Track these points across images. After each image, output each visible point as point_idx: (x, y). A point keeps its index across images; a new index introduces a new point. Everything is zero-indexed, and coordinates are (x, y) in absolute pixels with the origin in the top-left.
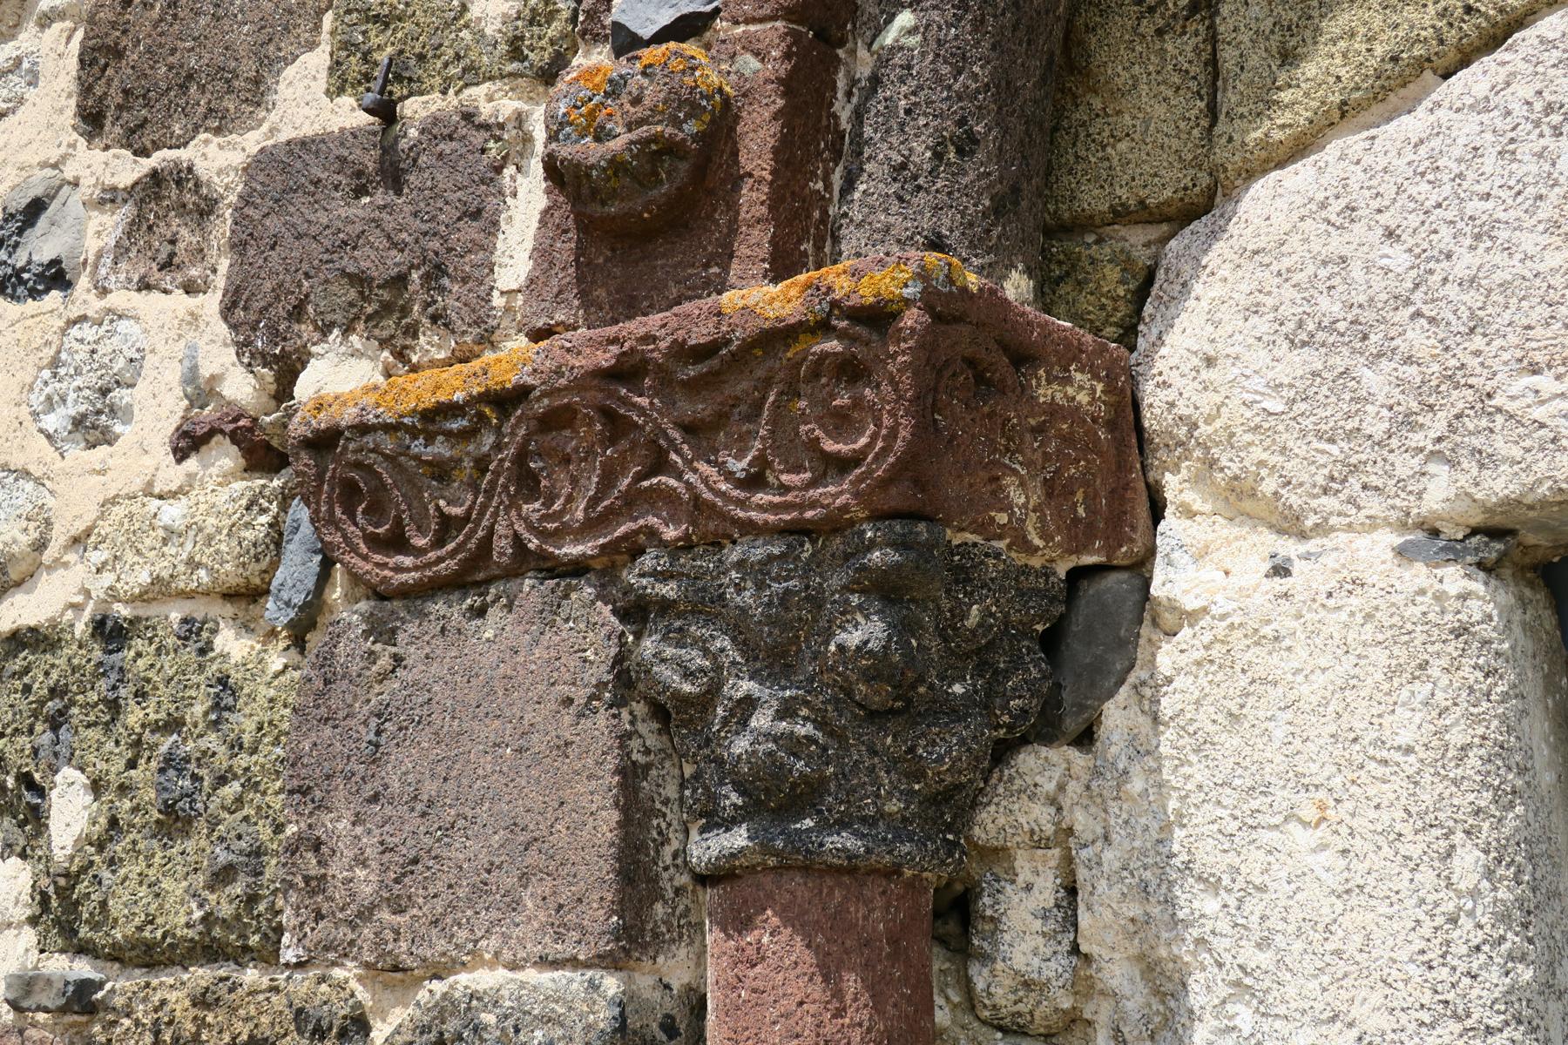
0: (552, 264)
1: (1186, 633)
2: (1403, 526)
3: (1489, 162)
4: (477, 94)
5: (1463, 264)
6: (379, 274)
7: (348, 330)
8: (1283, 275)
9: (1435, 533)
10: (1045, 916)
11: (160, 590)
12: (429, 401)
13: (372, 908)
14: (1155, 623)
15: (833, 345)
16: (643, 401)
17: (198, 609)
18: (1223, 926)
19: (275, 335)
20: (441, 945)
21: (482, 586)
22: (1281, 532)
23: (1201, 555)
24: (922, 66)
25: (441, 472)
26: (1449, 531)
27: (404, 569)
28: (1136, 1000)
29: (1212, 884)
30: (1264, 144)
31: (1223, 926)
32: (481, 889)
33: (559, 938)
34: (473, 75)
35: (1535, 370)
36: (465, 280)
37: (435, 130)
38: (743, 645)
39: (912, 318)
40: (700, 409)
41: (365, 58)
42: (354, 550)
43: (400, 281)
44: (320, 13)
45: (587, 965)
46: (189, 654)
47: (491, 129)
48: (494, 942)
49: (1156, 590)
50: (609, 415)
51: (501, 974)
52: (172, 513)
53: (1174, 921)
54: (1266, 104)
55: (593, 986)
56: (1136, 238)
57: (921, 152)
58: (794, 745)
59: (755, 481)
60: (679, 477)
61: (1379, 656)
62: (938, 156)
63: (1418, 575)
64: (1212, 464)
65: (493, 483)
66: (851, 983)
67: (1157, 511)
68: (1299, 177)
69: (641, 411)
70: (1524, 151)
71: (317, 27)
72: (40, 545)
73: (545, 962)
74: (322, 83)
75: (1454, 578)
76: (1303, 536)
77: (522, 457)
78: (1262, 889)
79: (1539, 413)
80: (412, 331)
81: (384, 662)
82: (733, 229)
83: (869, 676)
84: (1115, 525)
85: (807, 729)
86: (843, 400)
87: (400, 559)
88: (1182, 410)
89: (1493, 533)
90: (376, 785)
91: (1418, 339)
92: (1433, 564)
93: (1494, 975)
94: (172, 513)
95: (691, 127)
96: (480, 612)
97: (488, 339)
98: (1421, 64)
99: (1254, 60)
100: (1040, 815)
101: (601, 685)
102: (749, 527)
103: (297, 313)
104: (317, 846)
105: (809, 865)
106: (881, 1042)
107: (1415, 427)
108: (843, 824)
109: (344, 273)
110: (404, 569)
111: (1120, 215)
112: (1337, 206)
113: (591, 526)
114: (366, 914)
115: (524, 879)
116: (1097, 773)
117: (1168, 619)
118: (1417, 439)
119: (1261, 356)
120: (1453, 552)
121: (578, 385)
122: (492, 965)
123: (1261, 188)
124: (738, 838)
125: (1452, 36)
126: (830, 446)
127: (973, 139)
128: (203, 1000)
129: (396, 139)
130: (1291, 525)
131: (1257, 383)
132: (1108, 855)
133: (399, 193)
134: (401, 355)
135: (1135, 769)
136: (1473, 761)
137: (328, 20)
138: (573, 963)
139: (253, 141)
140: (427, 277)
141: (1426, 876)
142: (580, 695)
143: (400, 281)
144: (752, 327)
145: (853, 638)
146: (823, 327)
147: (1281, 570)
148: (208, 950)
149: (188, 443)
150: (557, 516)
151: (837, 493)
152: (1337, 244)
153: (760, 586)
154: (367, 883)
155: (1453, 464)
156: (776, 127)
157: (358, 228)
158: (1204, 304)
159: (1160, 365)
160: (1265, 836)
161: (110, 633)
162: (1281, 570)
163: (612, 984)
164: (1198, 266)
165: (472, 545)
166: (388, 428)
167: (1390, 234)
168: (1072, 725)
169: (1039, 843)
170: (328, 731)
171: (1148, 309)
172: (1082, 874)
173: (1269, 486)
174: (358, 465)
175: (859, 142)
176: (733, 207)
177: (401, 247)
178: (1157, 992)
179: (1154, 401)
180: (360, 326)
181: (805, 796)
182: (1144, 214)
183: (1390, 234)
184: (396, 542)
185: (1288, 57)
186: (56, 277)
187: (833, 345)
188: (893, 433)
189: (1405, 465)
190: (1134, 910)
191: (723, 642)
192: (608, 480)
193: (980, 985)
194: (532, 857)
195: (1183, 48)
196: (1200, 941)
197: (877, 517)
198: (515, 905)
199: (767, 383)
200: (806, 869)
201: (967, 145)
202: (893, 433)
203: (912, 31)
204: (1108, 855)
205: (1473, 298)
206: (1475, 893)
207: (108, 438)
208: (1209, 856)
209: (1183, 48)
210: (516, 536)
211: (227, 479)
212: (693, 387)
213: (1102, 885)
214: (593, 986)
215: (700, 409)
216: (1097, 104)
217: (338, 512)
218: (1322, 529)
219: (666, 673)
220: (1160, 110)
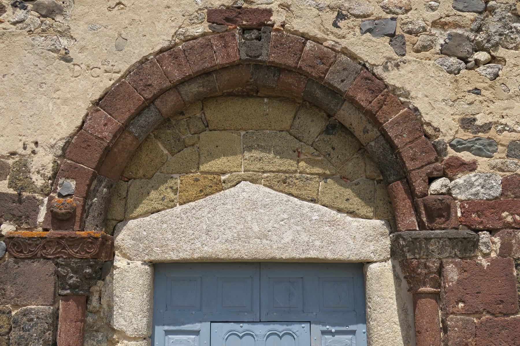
0: (47, 220)
1: (117, 269)
2: (142, 261)
3: (155, 225)
5: (152, 235)
6: (17, 215)
7: (10, 221)
8: (133, 232)
9: (145, 262)
10: (97, 299)
12: (31, 236)
13: (13, 298)
14: (113, 268)
15: (90, 240)
16: (63, 242)
18: (119, 301)
20: (25, 303)
21: (34, 259)
22: (129, 259)
23: (119, 261)
24: (97, 205)
26: (147, 262)
27: (22, 255)
29: (118, 297)
30: (132, 217)
31: (119, 301)
33: (44, 302)
35: (157, 247)
36: (32, 219)
37: (28, 198)
38: (71, 270)
39: (100, 239)
40: (71, 243)
41: (16, 184)
42: (14, 252)
43: (21, 217)
44: (7, 175)
45: (48, 305)
48: (34, 302)
49: (114, 264)
50: (58, 242)
51: (35, 306)
53: (113, 301)
54: (132, 212)
55: (50, 308)
56: (114, 223)
57: (96, 215)
58: (78, 282)
59: (77, 253)
60: (67, 251)
61: (139, 274)
62: (98, 215)
63: (143, 267)
64: (122, 251)
65: (39, 248)
66: (80, 308)
67: (114, 255)
68: (135, 221)
69: (63, 243)
70: (159, 225)
71: (6, 177)
73: (42, 305)
74: (7, 186)
75: (147, 267)
76: (131, 260)
77: (44, 245)
78: (123, 298)
79: (157, 252)
80: (22, 223)
81: (17, 266)
82: (75, 222)
83: (88, 275)
84: (110, 257)
85: (79, 280)
86: (90, 246)
87: (21, 254)
88: (119, 244)
89: (151, 262)
90: (15, 282)
91: (146, 242)
92: (145, 265)
93: (146, 307)
95: (72, 210)
96: (34, 262)
97: (36, 227)
98: (149, 212)
99: (131, 207)
100: (98, 288)
101: (52, 273)
102: (76, 258)
104: (4, 289)
105: (77, 295)
107: (145, 251)
108: (81, 290)
109: (10, 213)
111: (113, 219)
112: (139, 226)
113: (53, 254)
114: (12, 298)
115: (39, 295)
116: (105, 284)
117: (115, 268)
118: (145, 252)
119: (129, 241)
120: (147, 264)
121: (55, 238)
122: (33, 305)
123: (131, 222)
124: (69, 291)
125: (153, 210)
126: (88, 251)
127: (102, 213)
129: (21, 197)
130: (130, 259)
131: (128, 243)
132: (106, 293)
133: (21, 205)
134: (19, 226)
135: (110, 284)
136: (147, 286)
137: (8, 177)
138: (47, 305)
140: (25, 217)
141: (141, 297)
142: (49, 274)
143: (21, 217)
144: (80, 237)
146: (89, 238)
147: (129, 264)
150: (48, 252)
151: (88, 256)
152: (139, 230)
153: (76, 264)
154: (13, 294)
155: (148, 255)
156: (81, 211)
157: (14, 208)
158: (123, 233)
159: (117, 239)
160: (125, 292)
162: (129, 264)
163: (52, 308)
164: (122, 229)
165: (34, 254)
166: (23, 238)
167: (144, 230)
168: (102, 278)
169: (97, 291)
170: (6, 275)
171: (115, 232)
172: (102, 295)
173: (128, 255)
174: (16, 242)
175: (88, 212)
176: (75, 219)
177: (22, 212)
178: (109, 308)
179: (116, 243)
180: (12, 221)
181: (78, 287)
183: (144, 230)
184: (21, 252)
185: (135, 208)
187: (90, 240)
188: (96, 251)
189: (143, 255)
190: (108, 299)
191: (69, 269)
192: (56, 250)
193: (89, 307)
194: (41, 292)
195: (123, 202)
196: (116, 303)
197: (92, 258)
198: (38, 298)
199: (81, 243)
200: (76, 295)
201: (101, 214)
202: (96, 251)
203: (96, 200)
204: (106, 293)
205: (152, 239)
206: (145, 299)
208: (118, 294)
209: (123, 202)
210: (41, 254)
212: (70, 241)
213: (105, 296)
214: (50, 308)
215: (71, 243)
216: (111, 206)
217: (12, 247)
218: (133, 260)
219: (62, 272)
220: (119, 209)
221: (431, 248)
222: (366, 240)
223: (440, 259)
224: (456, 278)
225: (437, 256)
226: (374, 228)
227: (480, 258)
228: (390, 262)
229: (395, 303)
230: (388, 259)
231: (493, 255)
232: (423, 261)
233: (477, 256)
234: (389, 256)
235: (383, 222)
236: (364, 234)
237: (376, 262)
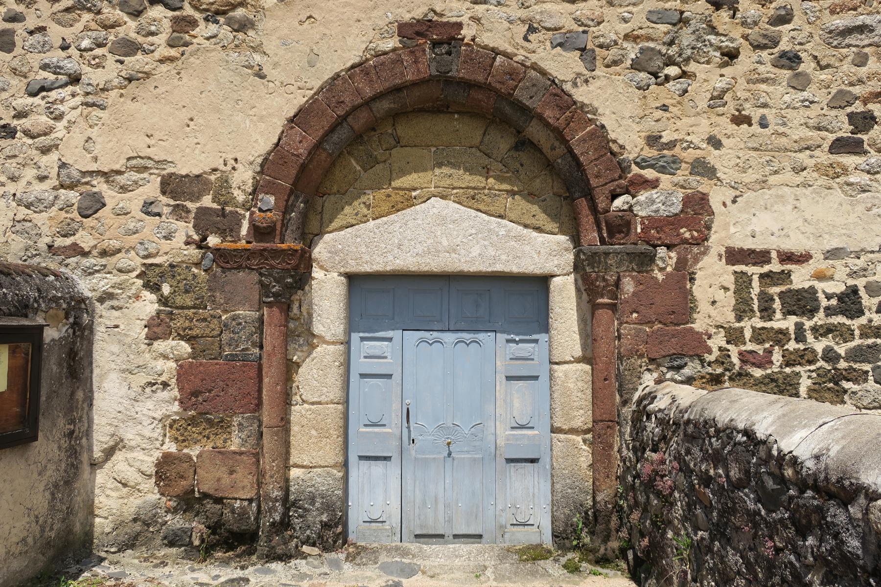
4: (238, 209)
5: (347, 248)
11: (183, 262)
17: (189, 265)
19: (203, 232)
25: (235, 256)
28: (306, 316)
32: (239, 303)
34: (237, 207)
43: (225, 230)
46: (187, 270)
47: (240, 214)
52: (185, 252)
54: (328, 227)
56: (311, 236)
59: (278, 264)
63: (339, 278)
68: (331, 235)
72: (158, 253)
75: (342, 278)
91: (342, 255)
94: (185, 252)
97: (240, 240)
103: (207, 230)
105: (280, 302)
106: (3, 303)
110: (229, 266)
111: (309, 233)
113: (257, 265)
120: (342, 276)
124: (272, 299)
128: (194, 313)
130: (327, 271)
137: (211, 192)
139: (198, 205)
143: (225, 230)
145: (289, 280)
146: (289, 250)
148: (194, 307)
149: (187, 243)
151: (289, 267)
154: (222, 301)
161: (172, 266)
169: (297, 300)
179: (313, 256)
181: (280, 295)
182: (312, 234)
184: (228, 262)
185: (331, 222)
186: (159, 215)
195: (319, 217)
201: (299, 228)
207: (170, 239)
208: (316, 303)
209: (319, 217)
211: (194, 249)
221: (609, 262)
222: (550, 254)
223: (618, 272)
224: (632, 290)
225: (615, 270)
226: (558, 243)
227: (656, 272)
228: (572, 275)
229: (576, 314)
230: (571, 273)
231: (669, 269)
232: (601, 274)
233: (653, 270)
234: (572, 270)
235: (568, 238)
236: (549, 249)
237: (559, 276)
